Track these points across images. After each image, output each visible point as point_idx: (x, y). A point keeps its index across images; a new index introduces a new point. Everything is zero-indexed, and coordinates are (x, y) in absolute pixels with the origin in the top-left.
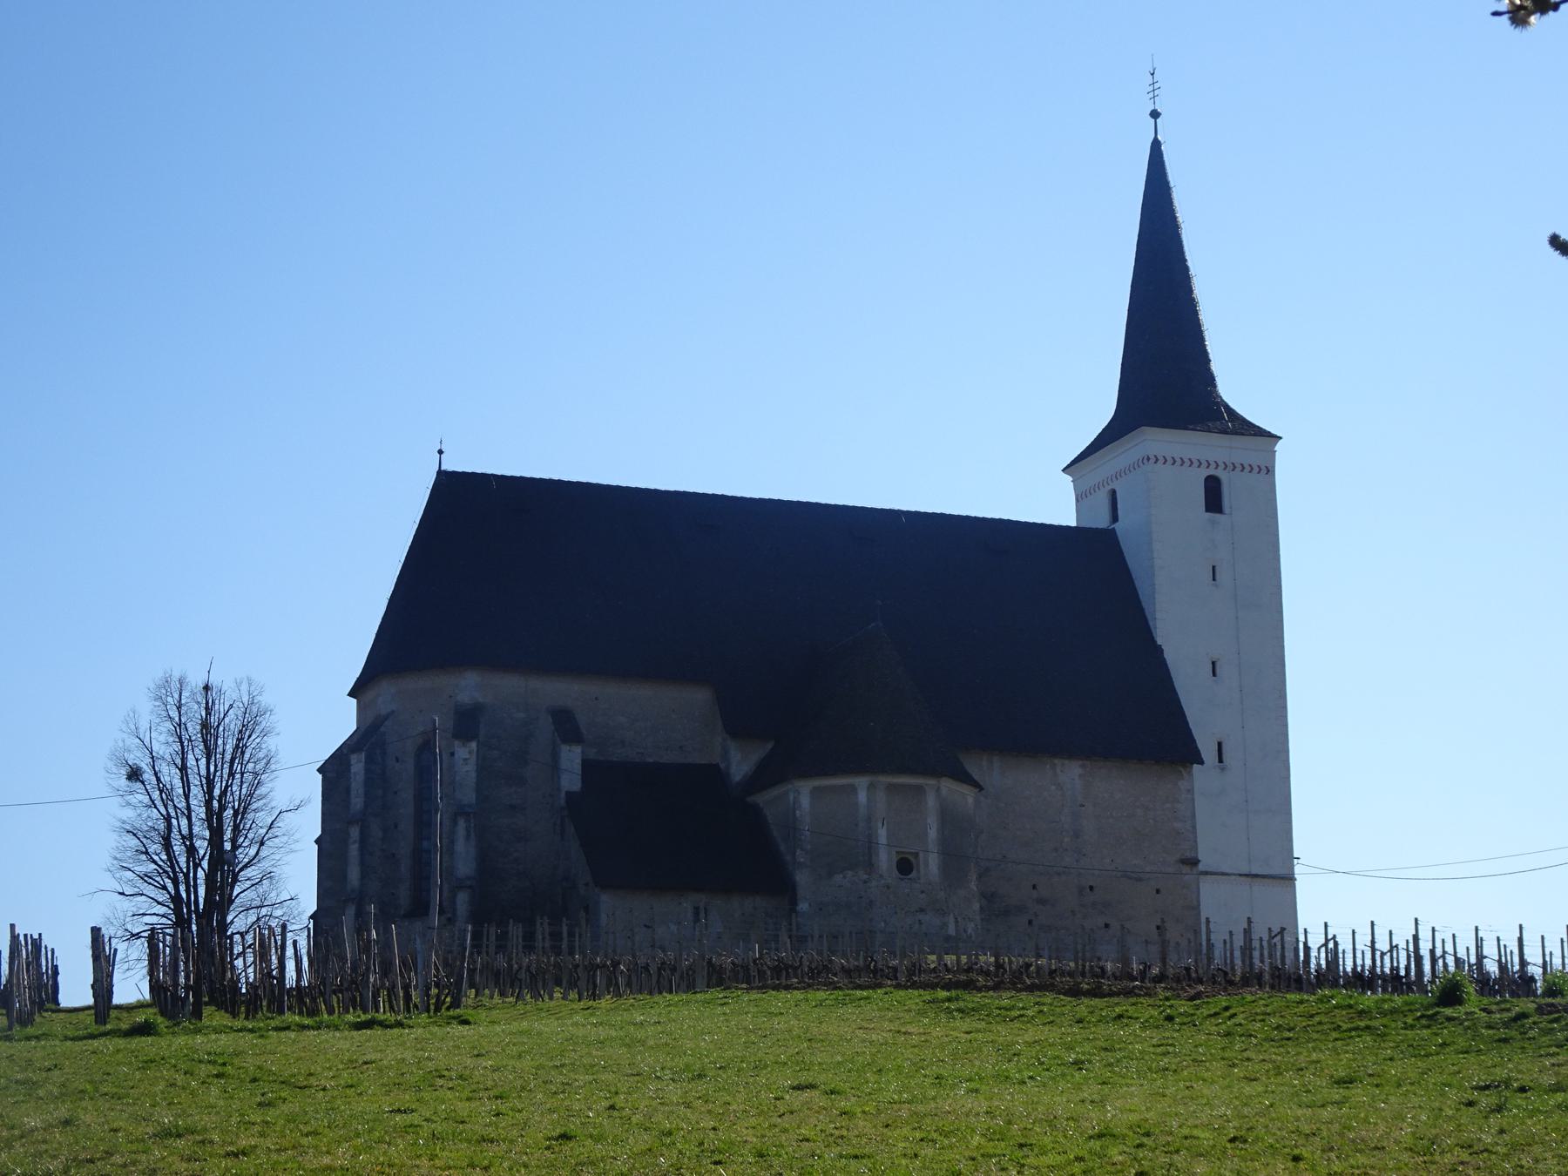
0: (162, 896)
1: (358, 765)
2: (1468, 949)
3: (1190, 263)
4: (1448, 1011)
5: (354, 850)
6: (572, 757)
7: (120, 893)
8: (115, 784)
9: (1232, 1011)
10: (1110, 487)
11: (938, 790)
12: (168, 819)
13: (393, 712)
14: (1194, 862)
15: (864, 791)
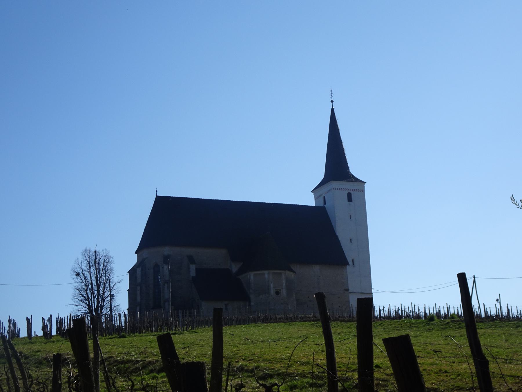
0: (85, 305)
1: (139, 270)
2: (433, 307)
3: (342, 139)
4: (432, 322)
5: (138, 292)
6: (193, 267)
7: (75, 305)
8: (73, 277)
9: (383, 324)
10: (323, 196)
11: (285, 273)
12: (86, 286)
13: (147, 257)
14: (348, 290)
15: (267, 274)
